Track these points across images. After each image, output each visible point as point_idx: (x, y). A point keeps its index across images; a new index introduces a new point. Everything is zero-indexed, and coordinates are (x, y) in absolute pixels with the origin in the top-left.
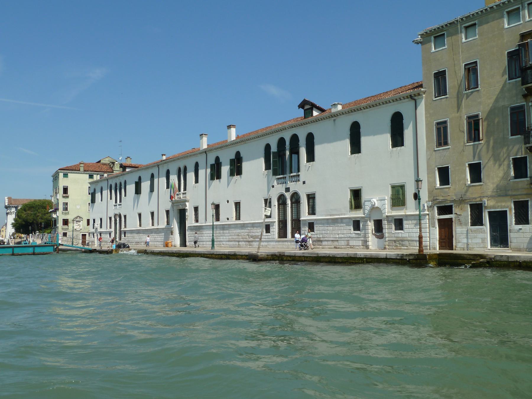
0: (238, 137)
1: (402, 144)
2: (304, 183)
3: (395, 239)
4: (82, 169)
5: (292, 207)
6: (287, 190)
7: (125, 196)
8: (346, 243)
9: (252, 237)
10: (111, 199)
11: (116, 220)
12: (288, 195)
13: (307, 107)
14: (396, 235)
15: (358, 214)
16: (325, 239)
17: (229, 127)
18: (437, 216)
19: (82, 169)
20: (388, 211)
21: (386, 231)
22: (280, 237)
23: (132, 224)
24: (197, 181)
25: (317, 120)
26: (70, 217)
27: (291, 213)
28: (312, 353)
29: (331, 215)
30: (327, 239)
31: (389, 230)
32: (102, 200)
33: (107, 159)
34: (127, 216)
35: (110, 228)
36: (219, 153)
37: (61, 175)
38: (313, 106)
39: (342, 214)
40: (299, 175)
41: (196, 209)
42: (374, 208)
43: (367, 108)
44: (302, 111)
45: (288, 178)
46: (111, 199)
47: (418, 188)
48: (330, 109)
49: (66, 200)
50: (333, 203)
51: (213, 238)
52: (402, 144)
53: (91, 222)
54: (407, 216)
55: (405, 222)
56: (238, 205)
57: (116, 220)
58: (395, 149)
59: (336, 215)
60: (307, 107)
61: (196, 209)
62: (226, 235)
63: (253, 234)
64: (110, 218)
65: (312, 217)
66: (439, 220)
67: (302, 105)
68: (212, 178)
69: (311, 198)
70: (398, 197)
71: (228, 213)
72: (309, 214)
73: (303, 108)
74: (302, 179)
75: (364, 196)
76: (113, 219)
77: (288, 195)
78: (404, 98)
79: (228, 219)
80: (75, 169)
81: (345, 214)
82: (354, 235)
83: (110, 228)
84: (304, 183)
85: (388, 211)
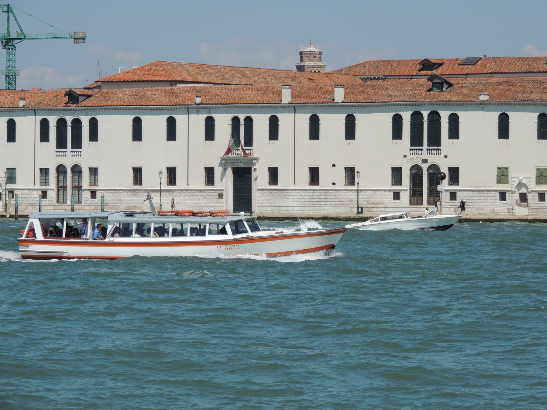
3: (538, 208)
9: (372, 203)
14: (540, 205)
15: (503, 187)
20: (533, 186)
28: (333, 283)
29: (476, 187)
30: (471, 207)
31: (533, 199)
39: (488, 187)
42: (521, 185)
45: (425, 151)
54: (402, 190)
55: (507, 195)
59: (482, 187)
63: (376, 201)
69: (94, 171)
73: (431, 81)
75: (511, 174)
81: (491, 187)
82: (500, 204)
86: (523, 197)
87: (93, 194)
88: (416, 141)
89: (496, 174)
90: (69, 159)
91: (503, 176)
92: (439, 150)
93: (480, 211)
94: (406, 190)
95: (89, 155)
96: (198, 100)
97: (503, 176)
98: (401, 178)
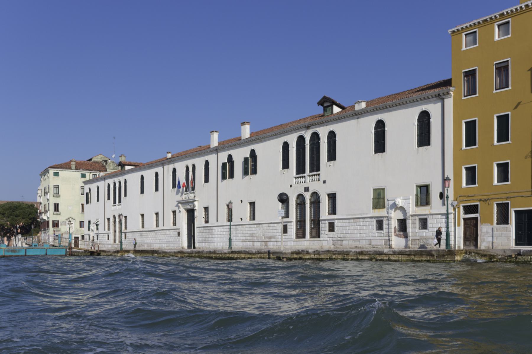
0: (251, 135)
1: (429, 144)
2: (324, 182)
3: (418, 238)
4: (73, 167)
5: (311, 207)
6: (307, 189)
7: (125, 195)
8: (368, 243)
10: (109, 199)
11: (120, 220)
12: (308, 196)
13: (326, 105)
14: (420, 234)
16: (345, 239)
17: (243, 124)
18: (463, 215)
19: (73, 167)
20: (412, 209)
21: (409, 230)
22: (298, 237)
23: (134, 224)
24: (207, 180)
25: (339, 119)
26: (60, 218)
27: (310, 214)
30: (348, 239)
31: (413, 228)
32: (98, 201)
33: (99, 157)
34: (128, 218)
35: (109, 229)
36: (233, 152)
37: (52, 171)
38: (334, 103)
39: (364, 214)
40: (319, 175)
41: (206, 209)
43: (393, 106)
44: (321, 108)
46: (109, 199)
47: (444, 186)
48: (354, 106)
49: (57, 200)
50: (355, 203)
51: (230, 237)
52: (429, 144)
53: (86, 224)
55: (429, 221)
56: (252, 204)
57: (120, 220)
58: (421, 148)
59: (358, 214)
60: (327, 103)
61: (206, 209)
62: (239, 235)
64: (109, 219)
65: (333, 217)
66: (465, 219)
67: (321, 103)
68: (224, 177)
69: (332, 197)
70: (424, 194)
71: (242, 212)
72: (329, 214)
73: (322, 105)
74: (322, 180)
75: (388, 195)
76: (112, 220)
77: (308, 196)
78: (433, 97)
79: (242, 219)
80: (66, 166)
83: (109, 229)
84: (324, 182)
85: (412, 209)
86: (403, 224)
87: (332, 227)
88: (300, 170)
89: (372, 197)
90: (118, 209)
91: (379, 199)
92: (319, 175)
93: (357, 244)
94: (197, 227)
95: (331, 177)
96: (169, 156)
97: (379, 199)
98: (319, 207)
